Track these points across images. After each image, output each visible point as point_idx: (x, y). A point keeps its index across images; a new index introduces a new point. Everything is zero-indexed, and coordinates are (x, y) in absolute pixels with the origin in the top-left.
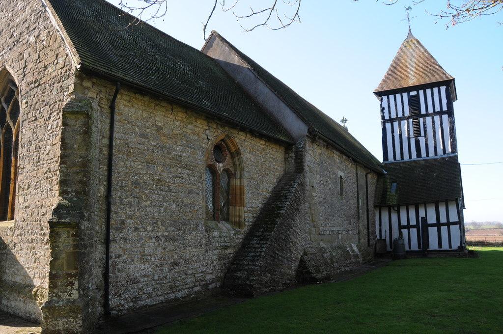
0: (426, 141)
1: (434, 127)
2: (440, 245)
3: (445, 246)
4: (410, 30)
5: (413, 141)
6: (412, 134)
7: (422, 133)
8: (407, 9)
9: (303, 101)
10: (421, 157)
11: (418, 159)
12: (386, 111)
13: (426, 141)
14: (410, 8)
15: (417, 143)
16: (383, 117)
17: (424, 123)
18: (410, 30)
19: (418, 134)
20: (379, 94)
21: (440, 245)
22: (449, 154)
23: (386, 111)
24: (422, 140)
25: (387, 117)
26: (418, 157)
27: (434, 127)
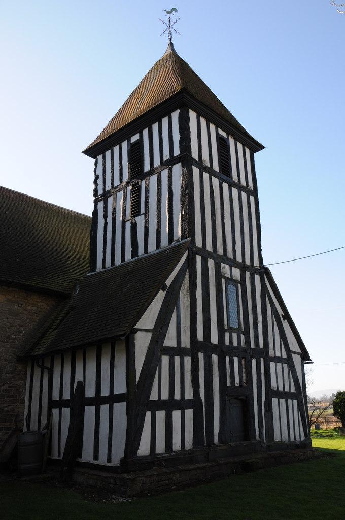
0: (146, 222)
1: (113, 176)
2: (96, 457)
3: (103, 460)
4: (171, 44)
5: (128, 226)
6: (128, 217)
7: (143, 211)
8: (169, 13)
9: (51, 208)
10: (137, 255)
11: (134, 259)
12: (100, 181)
13: (146, 222)
14: (174, 9)
15: (134, 227)
16: (96, 191)
17: (146, 187)
18: (171, 44)
19: (136, 212)
20: (93, 151)
21: (96, 457)
22: (178, 241)
23: (100, 181)
24: (140, 220)
25: (100, 192)
26: (122, 262)
27: (113, 176)
